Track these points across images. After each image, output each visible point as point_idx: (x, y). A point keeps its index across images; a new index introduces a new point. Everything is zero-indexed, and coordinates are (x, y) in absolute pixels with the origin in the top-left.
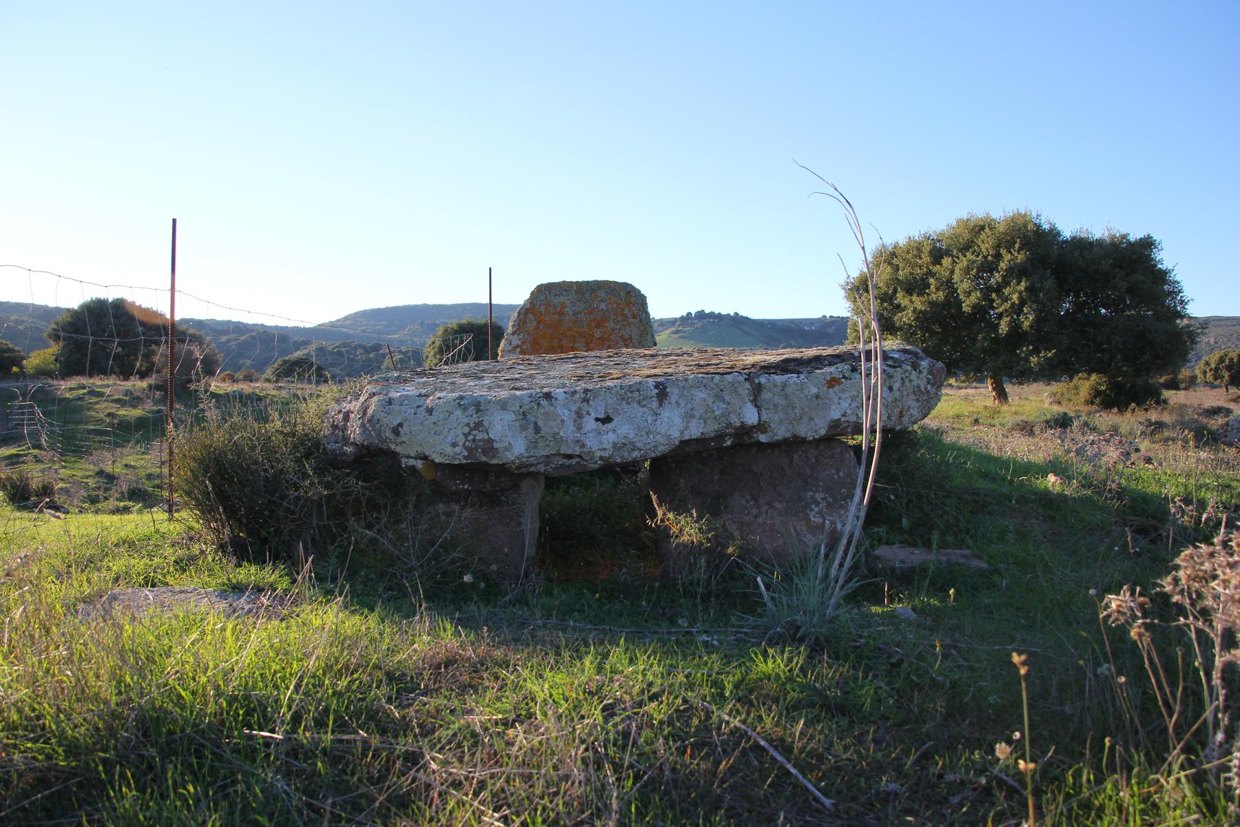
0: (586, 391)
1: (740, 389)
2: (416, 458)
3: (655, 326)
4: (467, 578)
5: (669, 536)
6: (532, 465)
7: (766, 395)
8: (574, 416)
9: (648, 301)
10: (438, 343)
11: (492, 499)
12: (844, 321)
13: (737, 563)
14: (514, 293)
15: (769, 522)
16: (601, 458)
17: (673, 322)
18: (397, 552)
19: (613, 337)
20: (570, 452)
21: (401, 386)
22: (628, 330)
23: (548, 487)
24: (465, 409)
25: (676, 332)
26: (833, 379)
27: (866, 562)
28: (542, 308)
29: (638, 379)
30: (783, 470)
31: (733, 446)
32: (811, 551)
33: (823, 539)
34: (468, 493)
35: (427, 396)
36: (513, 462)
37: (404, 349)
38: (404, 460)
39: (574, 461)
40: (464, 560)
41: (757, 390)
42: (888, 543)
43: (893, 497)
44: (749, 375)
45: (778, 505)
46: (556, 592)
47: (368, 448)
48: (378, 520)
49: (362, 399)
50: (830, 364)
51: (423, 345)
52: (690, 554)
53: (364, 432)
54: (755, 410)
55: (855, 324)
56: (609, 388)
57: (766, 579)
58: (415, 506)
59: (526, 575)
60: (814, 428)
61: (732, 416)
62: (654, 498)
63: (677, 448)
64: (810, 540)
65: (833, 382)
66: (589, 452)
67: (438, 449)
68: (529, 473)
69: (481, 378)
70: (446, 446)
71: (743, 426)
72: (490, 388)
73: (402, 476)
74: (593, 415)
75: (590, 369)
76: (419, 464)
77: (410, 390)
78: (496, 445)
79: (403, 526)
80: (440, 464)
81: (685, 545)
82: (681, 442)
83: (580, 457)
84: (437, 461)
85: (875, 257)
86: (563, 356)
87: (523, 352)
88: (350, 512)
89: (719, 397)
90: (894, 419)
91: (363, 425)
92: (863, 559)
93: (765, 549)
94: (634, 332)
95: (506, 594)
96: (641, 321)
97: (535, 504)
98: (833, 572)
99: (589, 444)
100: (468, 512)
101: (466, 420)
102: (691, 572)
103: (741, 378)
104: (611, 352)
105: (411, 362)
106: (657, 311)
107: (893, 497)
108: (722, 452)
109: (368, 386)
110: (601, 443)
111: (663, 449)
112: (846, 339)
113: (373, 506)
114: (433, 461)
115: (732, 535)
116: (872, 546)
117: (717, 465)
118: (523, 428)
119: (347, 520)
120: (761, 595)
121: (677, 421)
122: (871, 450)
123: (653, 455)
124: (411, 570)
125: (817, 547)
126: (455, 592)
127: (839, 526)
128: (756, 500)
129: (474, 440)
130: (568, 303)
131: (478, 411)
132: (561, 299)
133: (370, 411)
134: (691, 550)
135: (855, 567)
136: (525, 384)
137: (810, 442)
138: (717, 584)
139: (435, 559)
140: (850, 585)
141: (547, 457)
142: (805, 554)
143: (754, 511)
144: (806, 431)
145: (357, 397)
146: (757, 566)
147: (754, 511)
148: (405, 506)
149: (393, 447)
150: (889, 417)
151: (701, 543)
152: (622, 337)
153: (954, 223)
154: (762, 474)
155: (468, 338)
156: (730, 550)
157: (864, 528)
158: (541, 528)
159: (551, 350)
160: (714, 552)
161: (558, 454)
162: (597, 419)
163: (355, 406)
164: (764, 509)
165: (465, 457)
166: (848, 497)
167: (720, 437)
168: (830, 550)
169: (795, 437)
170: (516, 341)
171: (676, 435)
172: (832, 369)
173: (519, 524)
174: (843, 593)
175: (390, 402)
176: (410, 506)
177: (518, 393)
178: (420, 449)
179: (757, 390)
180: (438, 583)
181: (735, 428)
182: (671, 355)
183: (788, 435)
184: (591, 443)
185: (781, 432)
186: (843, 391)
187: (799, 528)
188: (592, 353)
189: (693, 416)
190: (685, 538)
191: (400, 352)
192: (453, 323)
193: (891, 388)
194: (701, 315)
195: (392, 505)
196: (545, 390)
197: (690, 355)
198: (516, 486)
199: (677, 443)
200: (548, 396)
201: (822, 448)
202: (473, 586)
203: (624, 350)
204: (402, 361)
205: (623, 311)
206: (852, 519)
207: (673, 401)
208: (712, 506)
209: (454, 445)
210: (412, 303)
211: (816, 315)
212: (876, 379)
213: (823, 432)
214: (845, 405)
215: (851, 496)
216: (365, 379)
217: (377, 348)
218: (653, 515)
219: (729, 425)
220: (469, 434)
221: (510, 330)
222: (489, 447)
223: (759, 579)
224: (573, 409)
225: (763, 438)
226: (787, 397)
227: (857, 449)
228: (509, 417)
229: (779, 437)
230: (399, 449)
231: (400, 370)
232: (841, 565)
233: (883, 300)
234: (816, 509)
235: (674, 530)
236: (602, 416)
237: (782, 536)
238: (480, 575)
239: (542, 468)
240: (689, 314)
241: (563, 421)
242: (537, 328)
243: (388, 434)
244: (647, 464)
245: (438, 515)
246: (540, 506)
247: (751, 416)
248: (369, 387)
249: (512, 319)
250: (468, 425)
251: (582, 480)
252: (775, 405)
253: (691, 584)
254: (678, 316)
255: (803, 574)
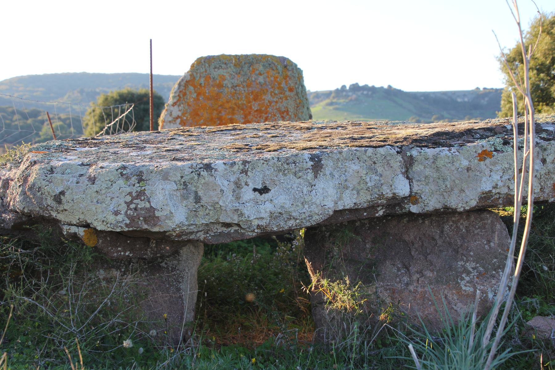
0: (245, 162)
1: (392, 162)
2: (78, 226)
3: (310, 99)
4: (127, 343)
5: (322, 302)
6: (192, 233)
7: (417, 168)
8: (233, 186)
9: (304, 75)
10: (98, 111)
11: (153, 266)
12: (497, 93)
13: (389, 330)
14: (175, 64)
15: (420, 290)
16: (258, 226)
17: (328, 94)
18: (56, 318)
19: (270, 110)
20: (228, 221)
21: (63, 155)
22: (285, 104)
23: (206, 254)
24: (128, 179)
25: (331, 104)
26: (484, 152)
27: (520, 333)
28: (202, 81)
29: (294, 151)
30: (434, 239)
31: (385, 217)
32: (462, 319)
33: (475, 308)
34: (129, 261)
35: (89, 165)
36: (173, 230)
37: (63, 116)
38: (65, 228)
39: (232, 230)
40: (124, 325)
41: (409, 163)
42: (542, 314)
43: (546, 268)
44: (401, 148)
45: (429, 274)
46: (213, 356)
47: (29, 216)
48: (37, 287)
49: (22, 167)
50: (482, 138)
51: (83, 113)
52: (343, 320)
53: (24, 199)
54: (407, 181)
55: (509, 96)
56: (267, 160)
57: (418, 347)
58: (76, 273)
59: (185, 340)
60: (471, 200)
61: (384, 187)
62: (308, 265)
63: (331, 217)
64: (461, 309)
65: (484, 155)
66: (247, 221)
67: (101, 217)
68: (190, 241)
69: (143, 149)
70: (107, 213)
71: (394, 197)
72: (151, 159)
73: (63, 243)
74: (252, 186)
75: (248, 141)
76: (81, 231)
77: (73, 159)
78: (157, 214)
79: (63, 292)
80: (101, 232)
81: (338, 312)
82: (335, 212)
83: (238, 225)
84: (99, 228)
85: (534, 27)
86: (223, 127)
87: (183, 123)
88: (7, 279)
89: (372, 169)
90: (547, 191)
91: (24, 193)
92: (516, 329)
93: (416, 316)
94: (291, 105)
95: (165, 359)
96: (297, 94)
97: (194, 270)
98: (485, 342)
99: (246, 213)
100: (129, 279)
101: (129, 190)
102: (344, 338)
103: (393, 152)
104: (269, 124)
105: (70, 132)
106: (313, 83)
107: (546, 268)
108: (373, 220)
109: (28, 153)
110: (258, 213)
111: (317, 219)
112: (499, 110)
113: (31, 271)
114: (95, 229)
115: (383, 301)
116: (525, 317)
117: (371, 234)
118: (184, 197)
119: (4, 287)
120: (413, 362)
121: (332, 192)
122: (522, 221)
123: (308, 224)
124: (70, 336)
125: (468, 316)
126: (113, 357)
127: (490, 296)
128: (407, 268)
129: (136, 209)
130: (227, 76)
131: (140, 180)
132: (221, 72)
133: (31, 180)
134: (346, 316)
135: (507, 337)
136: (186, 156)
137: (460, 213)
138: (370, 350)
139: (95, 325)
140: (503, 355)
141: (207, 225)
142: (456, 323)
143: (406, 279)
144: (458, 202)
145: (17, 164)
146: (409, 333)
147: (406, 279)
148: (66, 272)
149: (54, 214)
150: (542, 189)
151: (354, 310)
152: (279, 110)
153: (481, 89)
154: (413, 244)
155: (129, 109)
156: (382, 317)
157: (515, 297)
158: (199, 293)
159: (211, 121)
160: (367, 317)
161: (218, 223)
162: (255, 190)
163: (15, 173)
164: (415, 277)
165: (127, 225)
166: (499, 267)
167: (373, 207)
168: (482, 319)
169: (446, 208)
170: (176, 112)
171: (330, 206)
172: (484, 142)
173: (178, 290)
174: (496, 362)
175: (52, 170)
176: (71, 273)
177: (179, 164)
178: (82, 217)
179: (409, 163)
180: (97, 349)
181: (388, 199)
182: (326, 128)
183: (439, 206)
184: (250, 212)
185: (432, 203)
186: (494, 164)
187: (449, 295)
188: (250, 126)
189: (346, 188)
190: (339, 304)
191: (59, 119)
192: (114, 92)
193: (544, 161)
194: (355, 88)
195: (52, 273)
196: (206, 161)
197: (344, 128)
198: (176, 253)
199: (331, 213)
200: (208, 167)
201: (472, 218)
202: (132, 351)
203: (281, 123)
204: (62, 127)
205: (280, 84)
206: (503, 289)
207: (328, 173)
208: (365, 274)
209: (116, 213)
210: (72, 71)
211: (469, 86)
212: (529, 152)
213: (473, 203)
214: (496, 177)
215: (502, 266)
216: (25, 148)
217: (35, 114)
218: (308, 282)
219: (381, 196)
220: (131, 202)
221: (170, 101)
222: (151, 215)
223: (410, 346)
224: (232, 180)
225: (414, 209)
226: (438, 169)
227: (508, 220)
228: (171, 186)
229: (430, 208)
230: (60, 217)
231: (61, 138)
232: (493, 335)
233: (539, 71)
234: (467, 279)
235: (328, 296)
236: (260, 187)
237: (433, 304)
238: (139, 340)
239: (201, 236)
240: (344, 87)
241: (222, 191)
242: (197, 99)
243: (50, 201)
244: (302, 232)
245: (99, 281)
246: (199, 272)
247: (402, 188)
248: (30, 155)
249: (173, 91)
250: (130, 194)
251: (239, 246)
252: (426, 177)
253: (345, 349)
254: (333, 88)
255: (454, 342)
